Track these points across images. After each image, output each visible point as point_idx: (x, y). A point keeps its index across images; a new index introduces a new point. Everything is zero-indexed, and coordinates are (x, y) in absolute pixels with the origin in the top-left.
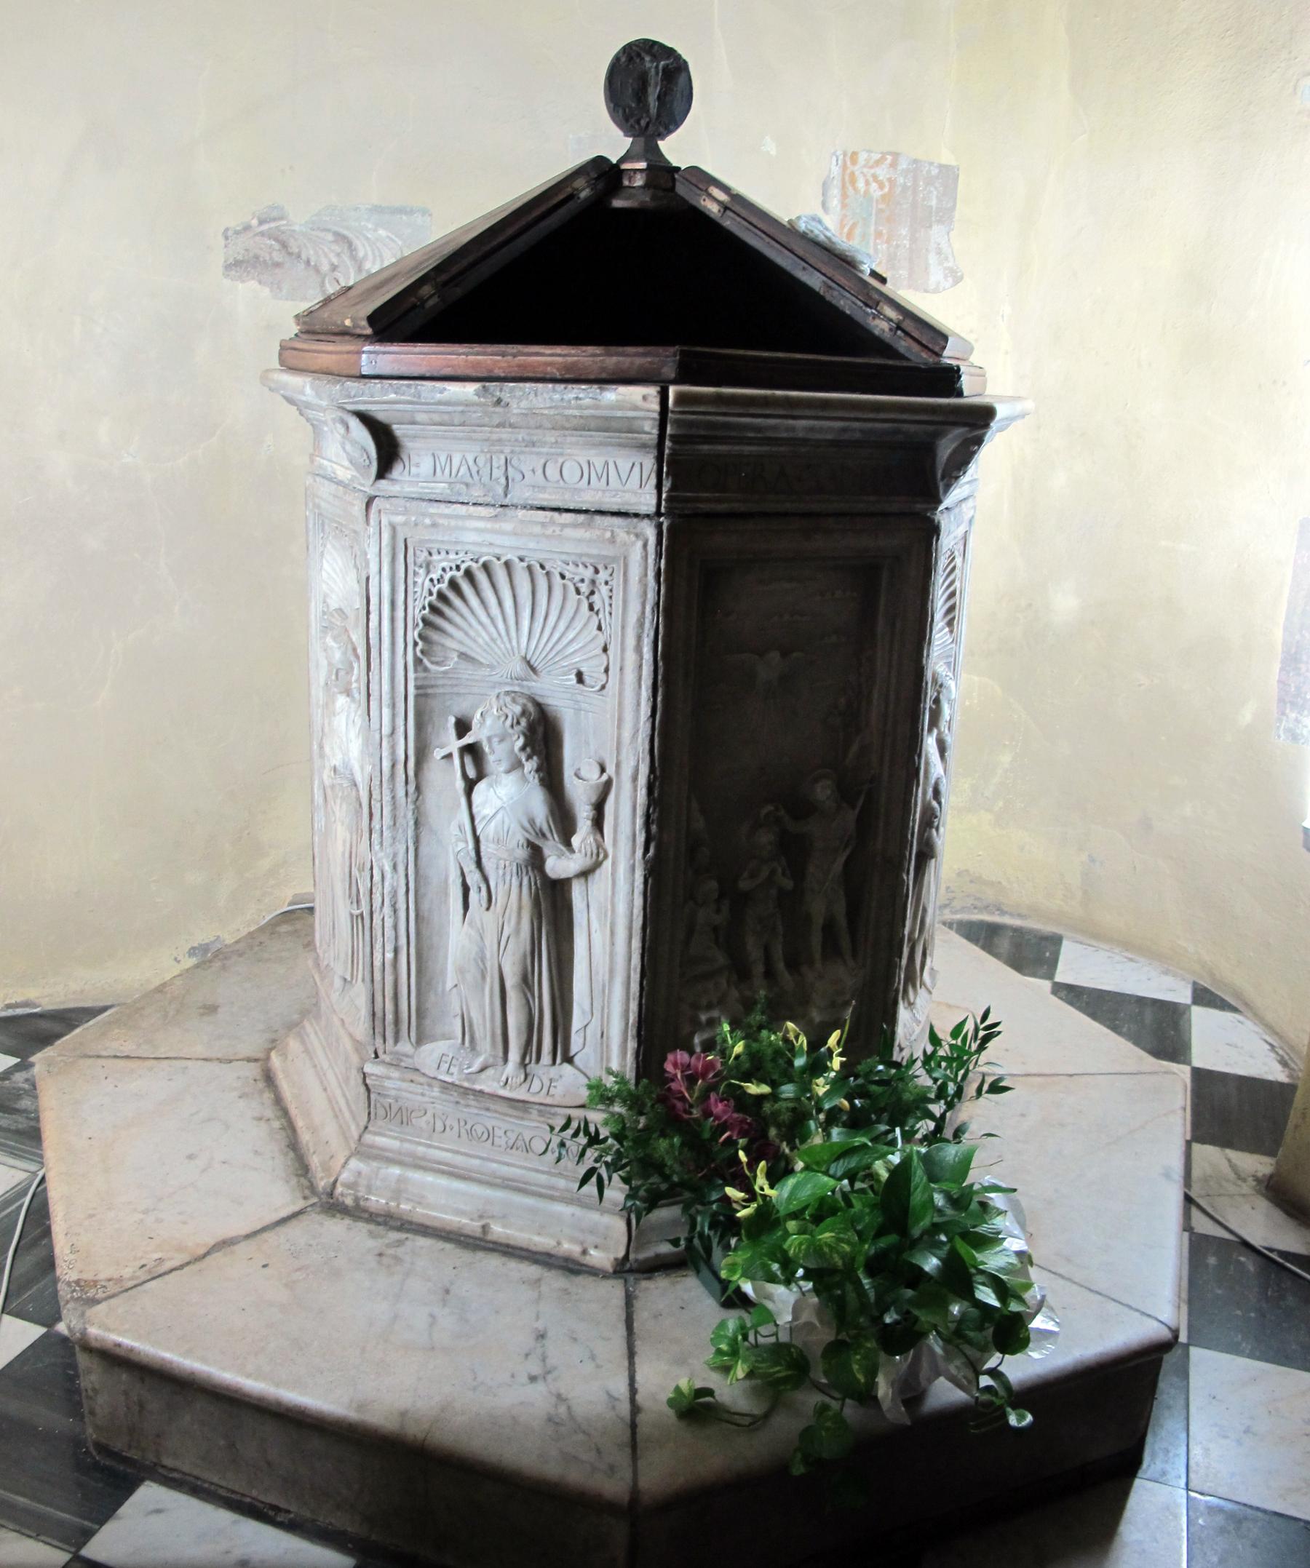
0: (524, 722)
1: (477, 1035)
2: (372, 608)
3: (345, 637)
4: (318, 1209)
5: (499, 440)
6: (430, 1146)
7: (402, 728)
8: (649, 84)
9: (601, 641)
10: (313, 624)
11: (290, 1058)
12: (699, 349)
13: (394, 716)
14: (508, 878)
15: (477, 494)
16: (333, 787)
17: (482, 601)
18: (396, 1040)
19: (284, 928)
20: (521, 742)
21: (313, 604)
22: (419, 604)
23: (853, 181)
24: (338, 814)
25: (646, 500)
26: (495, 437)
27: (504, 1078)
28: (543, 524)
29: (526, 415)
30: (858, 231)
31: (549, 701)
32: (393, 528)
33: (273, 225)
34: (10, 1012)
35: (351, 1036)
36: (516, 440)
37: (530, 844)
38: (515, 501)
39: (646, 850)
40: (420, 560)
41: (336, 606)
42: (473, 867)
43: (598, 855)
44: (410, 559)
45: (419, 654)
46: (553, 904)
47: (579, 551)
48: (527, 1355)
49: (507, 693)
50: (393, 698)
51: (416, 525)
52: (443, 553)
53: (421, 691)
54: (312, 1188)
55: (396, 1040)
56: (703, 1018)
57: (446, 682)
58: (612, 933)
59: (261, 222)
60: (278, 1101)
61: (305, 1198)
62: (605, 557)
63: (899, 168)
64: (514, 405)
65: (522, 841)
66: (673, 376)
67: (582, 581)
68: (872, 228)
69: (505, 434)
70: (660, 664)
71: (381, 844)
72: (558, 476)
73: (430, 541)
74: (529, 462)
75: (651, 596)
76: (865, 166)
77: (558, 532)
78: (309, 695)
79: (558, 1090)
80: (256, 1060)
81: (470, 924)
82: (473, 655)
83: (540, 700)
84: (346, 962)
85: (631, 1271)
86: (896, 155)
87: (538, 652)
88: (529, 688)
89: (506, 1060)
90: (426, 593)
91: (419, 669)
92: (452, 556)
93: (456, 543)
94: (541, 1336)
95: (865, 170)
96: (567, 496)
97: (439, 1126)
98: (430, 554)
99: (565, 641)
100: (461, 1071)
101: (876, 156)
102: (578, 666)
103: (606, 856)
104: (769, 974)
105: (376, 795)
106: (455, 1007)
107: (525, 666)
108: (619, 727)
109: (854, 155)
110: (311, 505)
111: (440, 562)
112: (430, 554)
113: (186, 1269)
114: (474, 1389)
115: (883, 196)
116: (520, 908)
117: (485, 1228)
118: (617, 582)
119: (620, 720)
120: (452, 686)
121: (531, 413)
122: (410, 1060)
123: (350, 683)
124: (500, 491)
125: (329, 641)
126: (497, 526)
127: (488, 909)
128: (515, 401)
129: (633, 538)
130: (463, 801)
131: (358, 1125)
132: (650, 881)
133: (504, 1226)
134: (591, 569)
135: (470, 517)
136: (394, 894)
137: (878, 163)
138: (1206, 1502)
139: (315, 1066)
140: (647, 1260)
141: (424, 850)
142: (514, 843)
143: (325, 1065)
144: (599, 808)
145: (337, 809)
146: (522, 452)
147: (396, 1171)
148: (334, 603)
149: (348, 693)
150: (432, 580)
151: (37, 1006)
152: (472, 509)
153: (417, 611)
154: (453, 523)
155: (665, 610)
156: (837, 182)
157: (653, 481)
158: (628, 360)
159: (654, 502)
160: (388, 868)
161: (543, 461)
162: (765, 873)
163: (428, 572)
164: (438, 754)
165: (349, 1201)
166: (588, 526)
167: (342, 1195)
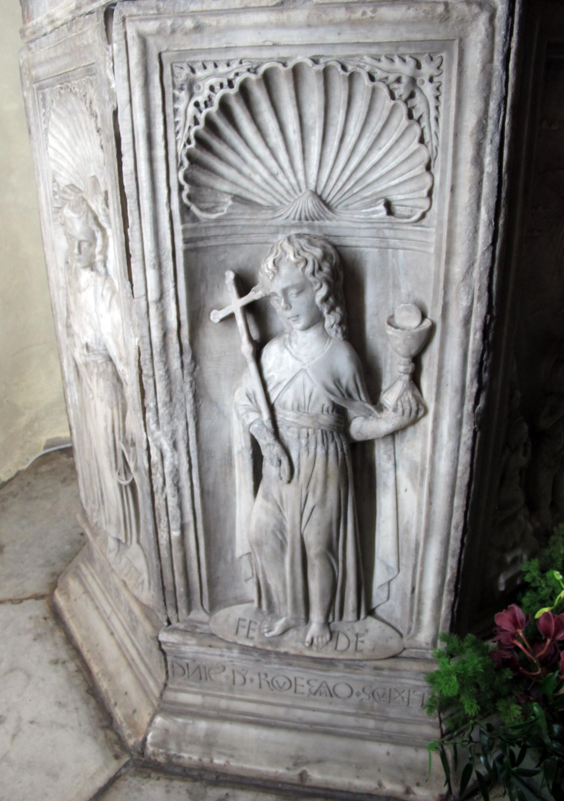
0: (326, 268)
1: (275, 599)
3: (84, 206)
4: (132, 770)
6: (232, 699)
7: (172, 291)
9: (424, 155)
10: (45, 208)
11: (72, 597)
14: (312, 447)
16: (86, 365)
18: (189, 609)
19: (44, 468)
20: (323, 292)
21: (42, 188)
22: (182, 138)
24: (95, 391)
27: (308, 638)
31: (348, 242)
32: (143, 40)
35: (137, 600)
41: (68, 183)
42: (270, 439)
43: (417, 412)
44: (168, 81)
45: (186, 200)
49: (299, 236)
51: (173, 31)
52: (210, 67)
53: (190, 245)
54: (120, 741)
55: (189, 609)
57: (218, 232)
58: (431, 493)
60: (69, 639)
61: (117, 757)
65: (327, 404)
70: (505, 177)
71: (157, 422)
73: (193, 52)
75: (496, 87)
77: (369, 14)
78: (48, 278)
80: (42, 597)
81: (266, 496)
84: (118, 524)
87: (332, 183)
88: (320, 227)
89: (307, 619)
91: (187, 218)
92: (222, 69)
97: (239, 679)
98: (193, 71)
99: (367, 165)
100: (262, 635)
102: (384, 195)
103: (426, 412)
106: (245, 569)
107: (317, 201)
108: (448, 261)
110: (27, 83)
111: (206, 79)
112: (193, 71)
117: (303, 775)
120: (226, 236)
122: (206, 627)
123: (93, 256)
125: (67, 212)
126: (284, 17)
127: (289, 482)
129: (475, 9)
130: (252, 366)
131: (156, 681)
132: (479, 434)
134: (411, 63)
136: (176, 472)
138: (525, 654)
139: (97, 608)
141: (205, 424)
142: (318, 408)
143: (108, 610)
144: (416, 361)
145: (94, 385)
147: (202, 725)
148: (64, 180)
149: (91, 266)
154: (223, 21)
155: (513, 107)
163: (191, 95)
164: (216, 316)
165: (161, 759)
167: (154, 754)
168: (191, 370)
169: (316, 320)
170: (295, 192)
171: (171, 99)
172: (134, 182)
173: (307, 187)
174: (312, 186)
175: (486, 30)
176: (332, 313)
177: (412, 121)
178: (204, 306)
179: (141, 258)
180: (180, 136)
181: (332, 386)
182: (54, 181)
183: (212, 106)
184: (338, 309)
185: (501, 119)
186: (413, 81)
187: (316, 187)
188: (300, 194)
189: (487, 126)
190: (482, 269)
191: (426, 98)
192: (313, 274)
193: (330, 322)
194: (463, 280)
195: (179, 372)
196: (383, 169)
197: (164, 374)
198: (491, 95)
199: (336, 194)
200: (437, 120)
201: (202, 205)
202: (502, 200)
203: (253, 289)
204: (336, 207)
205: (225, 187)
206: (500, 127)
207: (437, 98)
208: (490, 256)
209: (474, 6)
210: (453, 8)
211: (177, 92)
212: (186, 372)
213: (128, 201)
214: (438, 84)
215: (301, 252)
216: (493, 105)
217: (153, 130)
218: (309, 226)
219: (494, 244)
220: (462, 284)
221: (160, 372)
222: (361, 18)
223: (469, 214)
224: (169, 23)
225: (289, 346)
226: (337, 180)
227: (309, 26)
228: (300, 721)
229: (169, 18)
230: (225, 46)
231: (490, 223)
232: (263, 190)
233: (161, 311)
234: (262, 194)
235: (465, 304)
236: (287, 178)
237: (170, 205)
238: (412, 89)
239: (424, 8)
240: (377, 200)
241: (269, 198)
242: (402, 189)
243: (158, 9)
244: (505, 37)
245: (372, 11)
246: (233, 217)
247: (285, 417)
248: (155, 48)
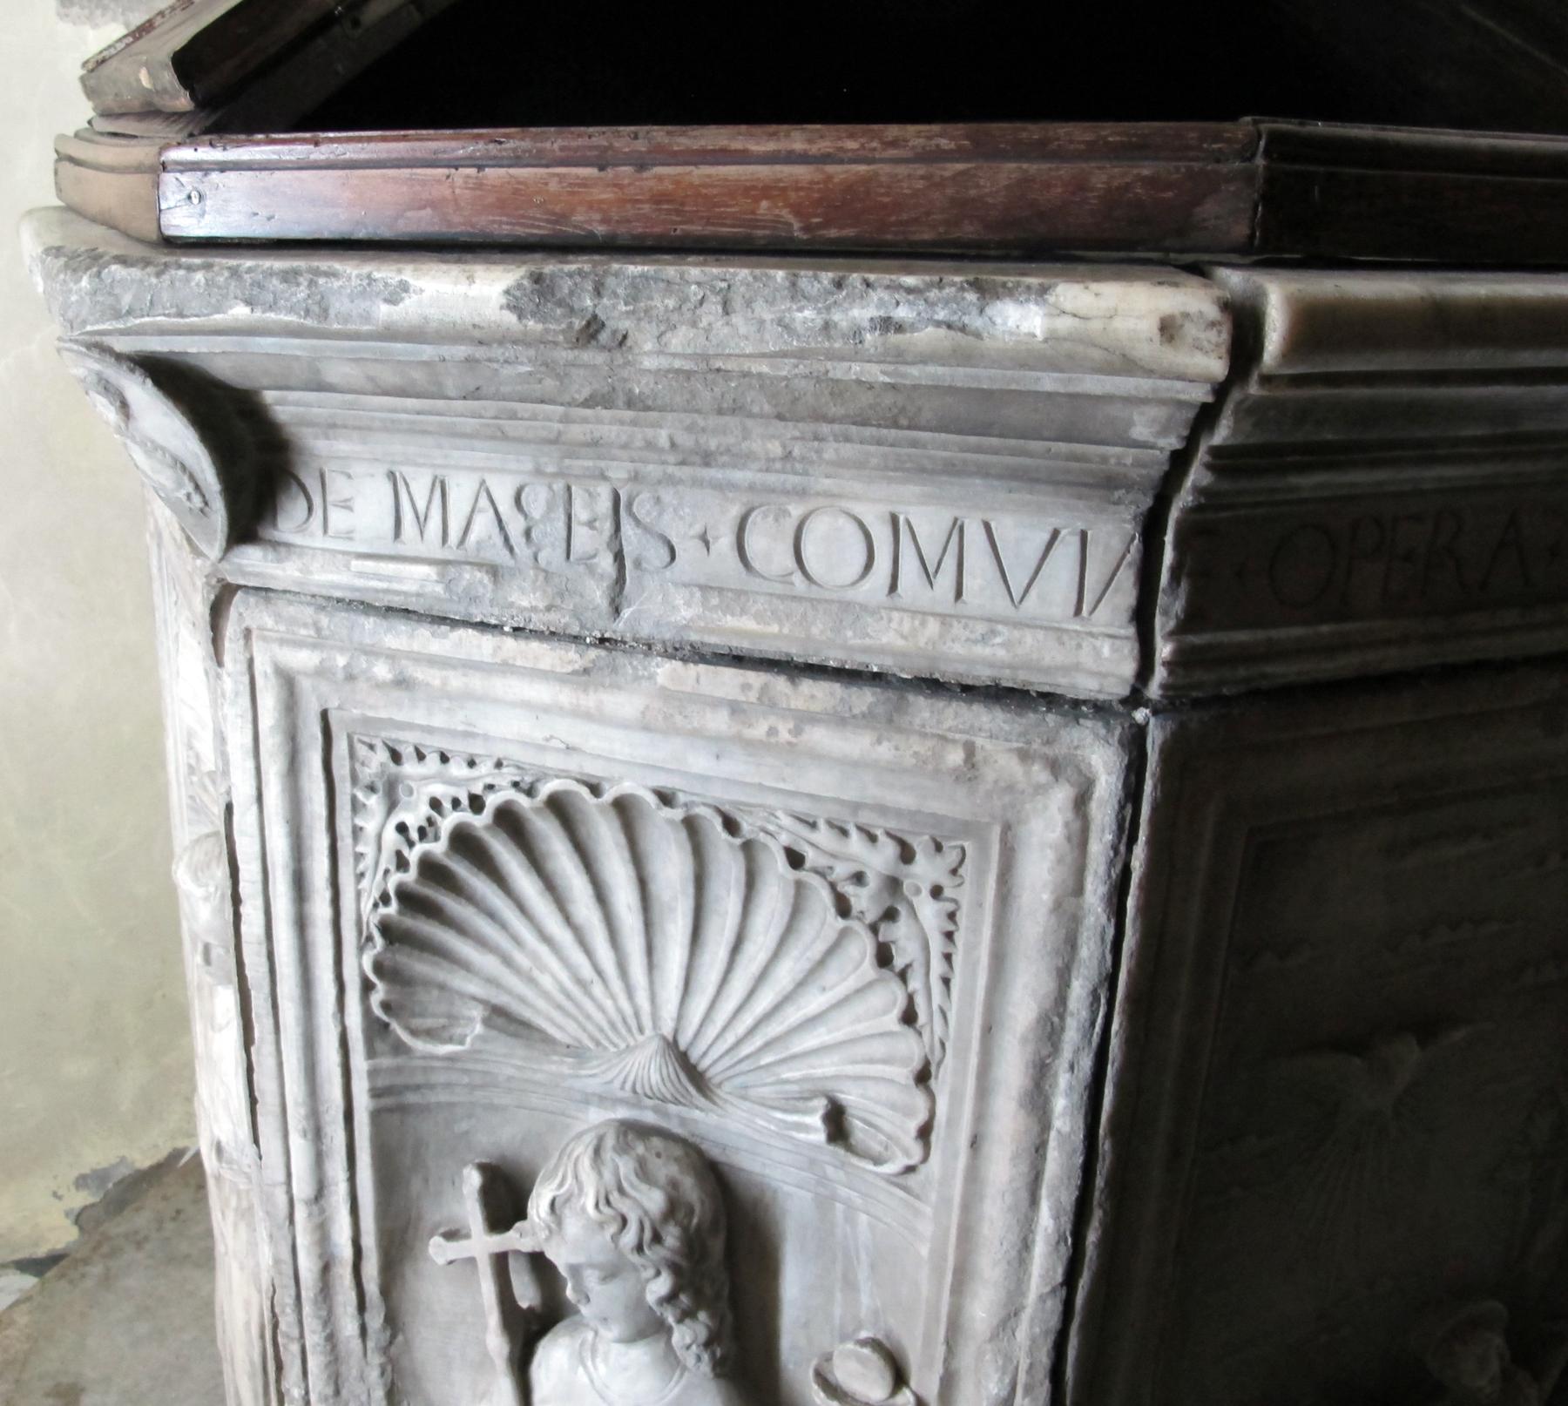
0: (672, 1236)
2: (245, 889)
5: (595, 443)
9: (911, 1048)
12: (1320, 128)
13: (319, 1159)
15: (525, 599)
17: (550, 885)
25: (1102, 659)
26: (576, 432)
28: (735, 709)
29: (688, 375)
32: (288, 683)
36: (650, 445)
38: (645, 630)
40: (369, 772)
45: (378, 1012)
47: (850, 795)
51: (350, 677)
52: (433, 760)
53: (388, 1101)
57: (454, 1077)
62: (938, 820)
64: (644, 341)
66: (1240, 231)
67: (859, 878)
69: (609, 425)
70: (1105, 1146)
72: (791, 563)
74: (689, 514)
75: (1090, 952)
82: (527, 1014)
83: (715, 1153)
87: (711, 1032)
88: (683, 1121)
90: (387, 860)
91: (380, 1046)
92: (457, 769)
93: (468, 735)
96: (819, 629)
98: (396, 757)
99: (792, 1015)
102: (829, 1086)
105: (287, 1322)
107: (672, 1068)
111: (425, 783)
112: (396, 757)
118: (976, 896)
120: (472, 1087)
121: (707, 369)
124: (597, 594)
126: (589, 700)
128: (651, 329)
129: (1040, 774)
134: (889, 850)
135: (506, 668)
146: (671, 481)
150: (402, 828)
153: (367, 906)
154: (456, 681)
155: (1130, 998)
157: (1125, 593)
158: (1065, 170)
159: (1129, 668)
161: (735, 511)
163: (392, 805)
166: (889, 723)
168: (384, 1344)
169: (649, 1328)
170: (629, 1030)
171: (348, 807)
172: (264, 960)
173: (655, 1026)
174: (667, 1029)
175: (1067, 825)
176: (687, 1321)
177: (885, 972)
178: (419, 1218)
179: (277, 1109)
180: (365, 883)
182: (190, 747)
183: (437, 838)
184: (702, 1316)
185: (1099, 1021)
186: (893, 884)
187: (676, 1032)
188: (640, 1038)
189: (1063, 1029)
190: (1037, 1330)
191: (922, 929)
192: (639, 1248)
193: (683, 1338)
194: (991, 1340)
195: (356, 1344)
196: (830, 1032)
197: (322, 1342)
198: (1076, 965)
199: (721, 1057)
200: (946, 982)
201: (417, 1022)
202: (1097, 1194)
203: (518, 1225)
204: (720, 1085)
206: (1096, 1039)
207: (949, 936)
208: (1059, 1308)
209: (1036, 767)
210: (985, 761)
211: (360, 795)
212: (371, 1344)
213: (253, 993)
214: (950, 907)
215: (615, 1197)
216: (1079, 991)
217: (307, 863)
218: (656, 1110)
219: (1070, 1280)
220: (989, 1347)
221: (313, 1338)
222: (764, 738)
223: (1010, 1209)
224: (341, 661)
225: (589, 1363)
226: (725, 1028)
227: (646, 728)
229: (342, 650)
230: (461, 728)
231: (1061, 1239)
232: (559, 1007)
233: (317, 1220)
234: (556, 1015)
235: (996, 1391)
236: (613, 997)
237: (341, 1018)
238: (888, 904)
239: (916, 748)
240: (814, 1095)
241: (572, 1027)
242: (873, 1090)
243: (318, 630)
244: (1115, 849)
245: (790, 732)
246: (485, 1057)
248: (314, 699)
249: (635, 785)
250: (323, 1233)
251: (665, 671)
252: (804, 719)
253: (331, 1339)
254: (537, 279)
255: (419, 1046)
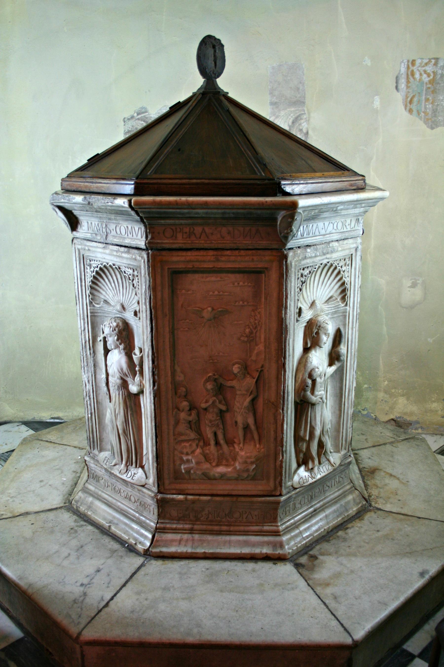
0: (117, 329)
6: (103, 492)
8: (211, 55)
9: (136, 298)
17: (109, 281)
18: (94, 449)
20: (116, 338)
23: (413, 74)
25: (142, 244)
28: (117, 251)
30: (415, 99)
33: (143, 115)
34: (52, 420)
37: (122, 378)
39: (154, 386)
46: (132, 402)
48: (88, 576)
50: (83, 316)
56: (185, 458)
59: (138, 114)
63: (439, 65)
68: (424, 97)
71: (84, 372)
75: (148, 282)
76: (419, 66)
79: (136, 478)
82: (108, 301)
83: (127, 321)
85: (149, 555)
86: (437, 59)
88: (124, 316)
89: (122, 463)
90: (90, 276)
91: (91, 305)
92: (98, 262)
94: (98, 571)
95: (420, 68)
98: (90, 261)
101: (426, 61)
104: (217, 443)
109: (413, 62)
111: (94, 264)
113: (8, 519)
114: (60, 583)
115: (430, 82)
116: (119, 403)
117: (110, 526)
119: (143, 332)
133: (115, 528)
135: (97, 247)
137: (426, 64)
140: (156, 553)
147: (91, 499)
151: (62, 420)
152: (98, 244)
156: (404, 76)
160: (87, 382)
161: (115, 226)
162: (211, 402)
163: (90, 268)
164: (99, 339)
165: (75, 507)
166: (128, 252)
181: (120, 371)
205: (102, 297)
228: (118, 507)
247: (110, 379)
249: (111, 263)
250: (85, 337)
251: (111, 247)
252: (122, 252)
253: (86, 355)
254: (85, 197)
255: (96, 305)
